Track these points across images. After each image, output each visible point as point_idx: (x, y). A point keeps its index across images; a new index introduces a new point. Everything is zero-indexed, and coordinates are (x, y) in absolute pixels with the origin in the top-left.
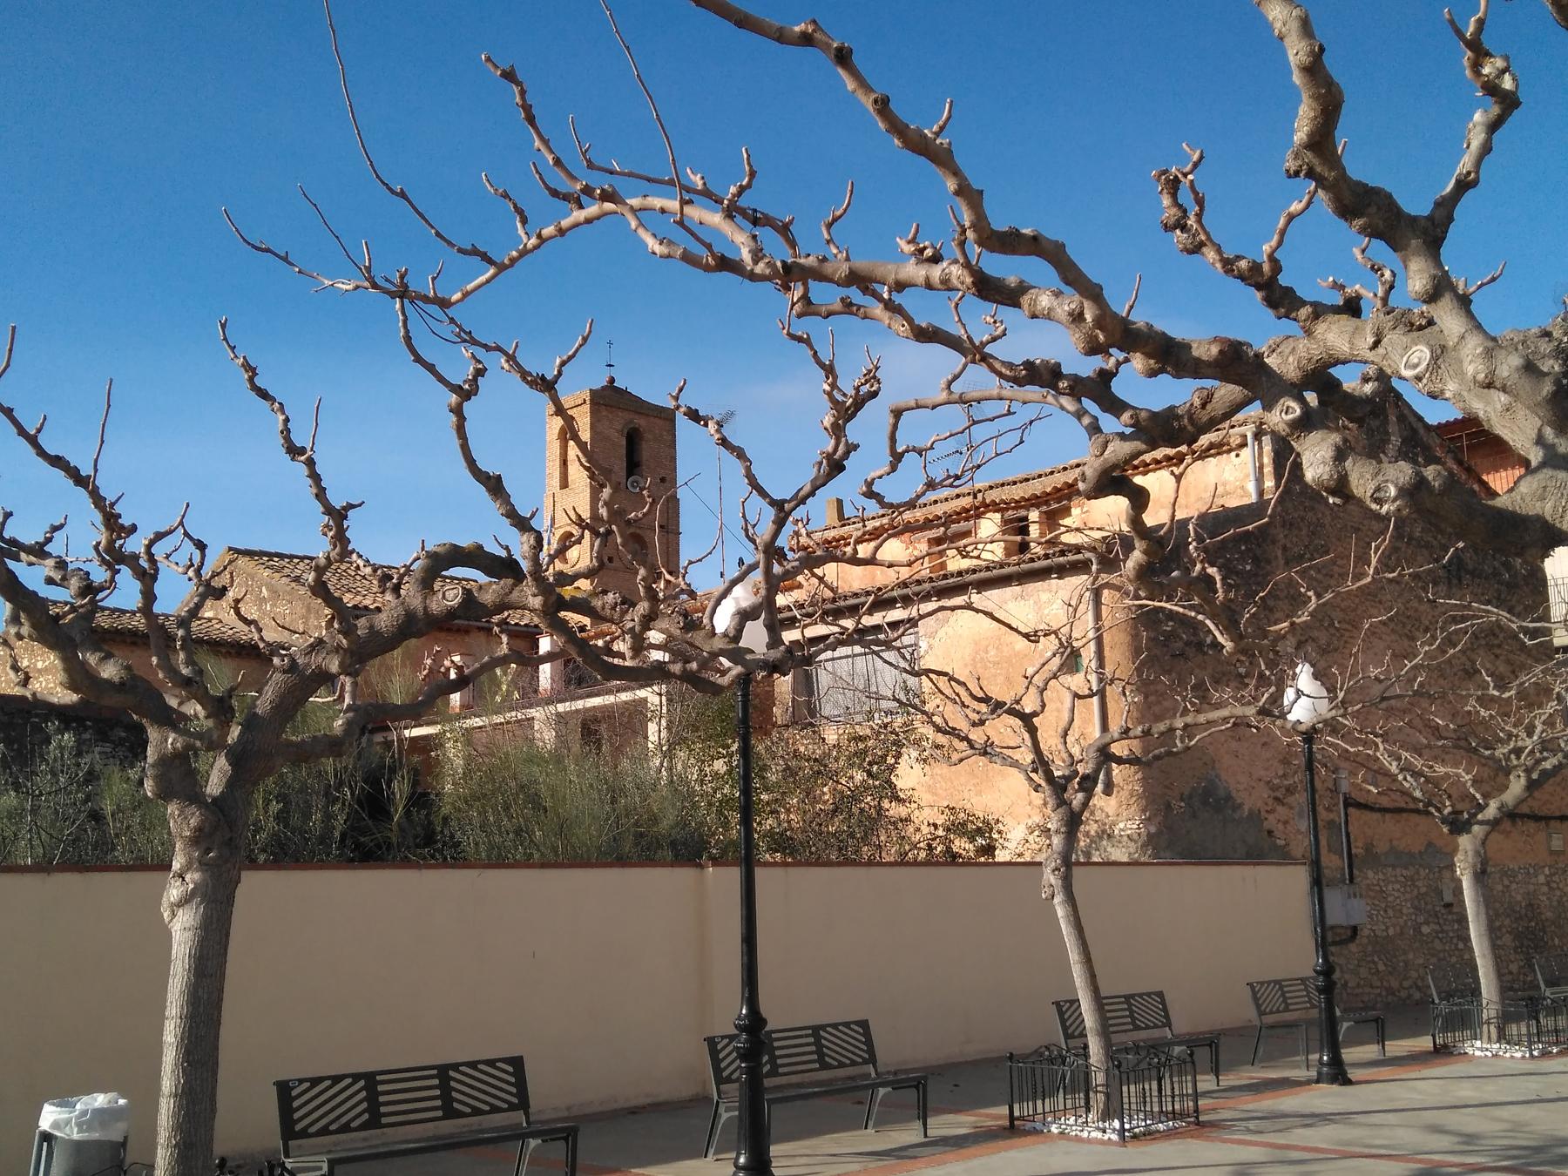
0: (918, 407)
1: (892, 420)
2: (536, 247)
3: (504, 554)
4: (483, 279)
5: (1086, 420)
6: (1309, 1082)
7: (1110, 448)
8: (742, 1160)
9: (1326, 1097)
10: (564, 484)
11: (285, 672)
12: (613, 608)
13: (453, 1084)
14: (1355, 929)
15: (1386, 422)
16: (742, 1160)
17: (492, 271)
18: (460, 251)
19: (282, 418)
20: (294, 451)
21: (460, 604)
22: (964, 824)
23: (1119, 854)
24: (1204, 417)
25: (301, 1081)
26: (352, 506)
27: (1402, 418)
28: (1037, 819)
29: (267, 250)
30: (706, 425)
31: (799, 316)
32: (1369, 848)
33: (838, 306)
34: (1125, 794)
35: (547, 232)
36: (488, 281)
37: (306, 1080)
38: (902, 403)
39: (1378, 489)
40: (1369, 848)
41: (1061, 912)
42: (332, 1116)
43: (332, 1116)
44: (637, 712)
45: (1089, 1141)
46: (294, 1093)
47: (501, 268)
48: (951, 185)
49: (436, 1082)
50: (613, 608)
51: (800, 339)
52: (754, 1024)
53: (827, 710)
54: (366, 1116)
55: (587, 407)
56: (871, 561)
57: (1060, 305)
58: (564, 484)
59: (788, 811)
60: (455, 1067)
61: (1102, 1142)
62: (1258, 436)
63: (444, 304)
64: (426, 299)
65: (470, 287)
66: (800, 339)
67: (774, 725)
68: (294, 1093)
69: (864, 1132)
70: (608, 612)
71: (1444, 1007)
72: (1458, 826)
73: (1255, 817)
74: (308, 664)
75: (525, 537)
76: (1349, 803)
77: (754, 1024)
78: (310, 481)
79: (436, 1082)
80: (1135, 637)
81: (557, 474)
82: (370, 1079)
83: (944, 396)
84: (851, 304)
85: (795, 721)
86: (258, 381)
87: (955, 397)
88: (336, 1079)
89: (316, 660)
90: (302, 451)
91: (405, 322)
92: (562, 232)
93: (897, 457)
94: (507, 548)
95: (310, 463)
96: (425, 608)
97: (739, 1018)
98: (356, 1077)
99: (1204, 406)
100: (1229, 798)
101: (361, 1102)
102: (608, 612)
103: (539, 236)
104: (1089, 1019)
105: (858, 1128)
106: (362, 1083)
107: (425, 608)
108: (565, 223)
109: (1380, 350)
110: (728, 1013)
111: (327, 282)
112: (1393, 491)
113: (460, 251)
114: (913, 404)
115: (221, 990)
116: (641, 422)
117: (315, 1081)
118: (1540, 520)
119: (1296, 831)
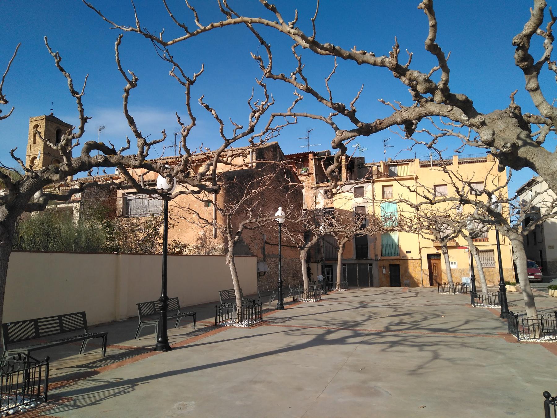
0: (281, 115)
1: (271, 118)
2: (209, 29)
3: (111, 147)
4: (183, 37)
5: (334, 126)
6: (274, 310)
7: (344, 134)
8: (160, 339)
9: (279, 313)
10: (34, 142)
11: (33, 178)
12: (160, 168)
13: (63, 321)
14: (265, 273)
15: (277, 153)
16: (160, 339)
17: (187, 35)
18: (179, 25)
19: (69, 79)
20: (74, 93)
21: (103, 161)
22: (178, 245)
23: (217, 253)
24: (379, 127)
25: (11, 323)
26: (88, 118)
27: (280, 153)
28: (195, 244)
29: (92, 8)
30: (211, 111)
31: (268, 77)
32: (268, 253)
33: (280, 76)
34: (219, 238)
35: (216, 24)
36: (185, 39)
37: (13, 323)
38: (276, 114)
39: (505, 144)
40: (268, 253)
41: (231, 267)
42: (24, 334)
43: (24, 334)
44: (71, 209)
45: (238, 327)
46: (9, 328)
47: (192, 35)
48: (431, 23)
49: (58, 321)
50: (160, 168)
51: (263, 85)
52: (165, 299)
53: (133, 213)
54: (35, 334)
55: (44, 121)
56: (230, 164)
57: (421, 76)
58: (34, 142)
59: (119, 240)
60: (64, 316)
61: (242, 328)
62: (252, 152)
63: (165, 44)
64: (159, 41)
65: (177, 40)
66: (263, 85)
67: (116, 216)
68: (9, 328)
69: (175, 329)
70: (158, 169)
71: (291, 290)
72: (302, 248)
73: (247, 245)
74: (43, 176)
75: (140, 140)
76: (266, 243)
77: (165, 299)
78: (78, 106)
79: (58, 321)
80: (225, 199)
81: (32, 139)
82: (36, 321)
83: (289, 113)
84: (284, 77)
85: (123, 216)
86: (60, 64)
87: (293, 114)
88: (24, 322)
89: (46, 175)
90: (77, 93)
91: (118, 54)
92: (222, 25)
93: (267, 130)
94: (113, 146)
95: (79, 99)
96: (89, 161)
97: (161, 298)
98: (31, 321)
99: (380, 124)
100: (242, 240)
101: (10, 329)
102: (158, 169)
103: (212, 25)
104: (237, 295)
105: (173, 327)
106: (33, 323)
107: (89, 161)
108: (224, 22)
109: (452, 112)
110: (158, 295)
111: (117, 26)
112: (509, 145)
113: (179, 25)
114: (279, 114)
115: (4, 292)
116: (61, 127)
117: (16, 323)
118: (525, 159)
119: (255, 247)
